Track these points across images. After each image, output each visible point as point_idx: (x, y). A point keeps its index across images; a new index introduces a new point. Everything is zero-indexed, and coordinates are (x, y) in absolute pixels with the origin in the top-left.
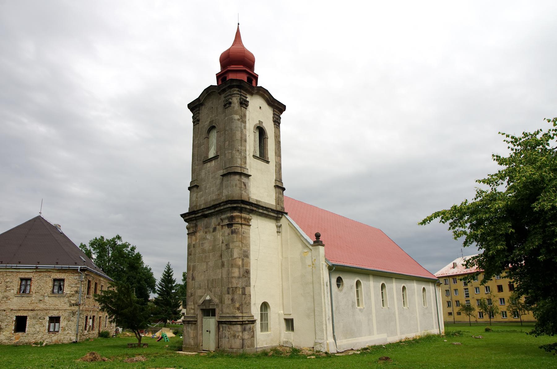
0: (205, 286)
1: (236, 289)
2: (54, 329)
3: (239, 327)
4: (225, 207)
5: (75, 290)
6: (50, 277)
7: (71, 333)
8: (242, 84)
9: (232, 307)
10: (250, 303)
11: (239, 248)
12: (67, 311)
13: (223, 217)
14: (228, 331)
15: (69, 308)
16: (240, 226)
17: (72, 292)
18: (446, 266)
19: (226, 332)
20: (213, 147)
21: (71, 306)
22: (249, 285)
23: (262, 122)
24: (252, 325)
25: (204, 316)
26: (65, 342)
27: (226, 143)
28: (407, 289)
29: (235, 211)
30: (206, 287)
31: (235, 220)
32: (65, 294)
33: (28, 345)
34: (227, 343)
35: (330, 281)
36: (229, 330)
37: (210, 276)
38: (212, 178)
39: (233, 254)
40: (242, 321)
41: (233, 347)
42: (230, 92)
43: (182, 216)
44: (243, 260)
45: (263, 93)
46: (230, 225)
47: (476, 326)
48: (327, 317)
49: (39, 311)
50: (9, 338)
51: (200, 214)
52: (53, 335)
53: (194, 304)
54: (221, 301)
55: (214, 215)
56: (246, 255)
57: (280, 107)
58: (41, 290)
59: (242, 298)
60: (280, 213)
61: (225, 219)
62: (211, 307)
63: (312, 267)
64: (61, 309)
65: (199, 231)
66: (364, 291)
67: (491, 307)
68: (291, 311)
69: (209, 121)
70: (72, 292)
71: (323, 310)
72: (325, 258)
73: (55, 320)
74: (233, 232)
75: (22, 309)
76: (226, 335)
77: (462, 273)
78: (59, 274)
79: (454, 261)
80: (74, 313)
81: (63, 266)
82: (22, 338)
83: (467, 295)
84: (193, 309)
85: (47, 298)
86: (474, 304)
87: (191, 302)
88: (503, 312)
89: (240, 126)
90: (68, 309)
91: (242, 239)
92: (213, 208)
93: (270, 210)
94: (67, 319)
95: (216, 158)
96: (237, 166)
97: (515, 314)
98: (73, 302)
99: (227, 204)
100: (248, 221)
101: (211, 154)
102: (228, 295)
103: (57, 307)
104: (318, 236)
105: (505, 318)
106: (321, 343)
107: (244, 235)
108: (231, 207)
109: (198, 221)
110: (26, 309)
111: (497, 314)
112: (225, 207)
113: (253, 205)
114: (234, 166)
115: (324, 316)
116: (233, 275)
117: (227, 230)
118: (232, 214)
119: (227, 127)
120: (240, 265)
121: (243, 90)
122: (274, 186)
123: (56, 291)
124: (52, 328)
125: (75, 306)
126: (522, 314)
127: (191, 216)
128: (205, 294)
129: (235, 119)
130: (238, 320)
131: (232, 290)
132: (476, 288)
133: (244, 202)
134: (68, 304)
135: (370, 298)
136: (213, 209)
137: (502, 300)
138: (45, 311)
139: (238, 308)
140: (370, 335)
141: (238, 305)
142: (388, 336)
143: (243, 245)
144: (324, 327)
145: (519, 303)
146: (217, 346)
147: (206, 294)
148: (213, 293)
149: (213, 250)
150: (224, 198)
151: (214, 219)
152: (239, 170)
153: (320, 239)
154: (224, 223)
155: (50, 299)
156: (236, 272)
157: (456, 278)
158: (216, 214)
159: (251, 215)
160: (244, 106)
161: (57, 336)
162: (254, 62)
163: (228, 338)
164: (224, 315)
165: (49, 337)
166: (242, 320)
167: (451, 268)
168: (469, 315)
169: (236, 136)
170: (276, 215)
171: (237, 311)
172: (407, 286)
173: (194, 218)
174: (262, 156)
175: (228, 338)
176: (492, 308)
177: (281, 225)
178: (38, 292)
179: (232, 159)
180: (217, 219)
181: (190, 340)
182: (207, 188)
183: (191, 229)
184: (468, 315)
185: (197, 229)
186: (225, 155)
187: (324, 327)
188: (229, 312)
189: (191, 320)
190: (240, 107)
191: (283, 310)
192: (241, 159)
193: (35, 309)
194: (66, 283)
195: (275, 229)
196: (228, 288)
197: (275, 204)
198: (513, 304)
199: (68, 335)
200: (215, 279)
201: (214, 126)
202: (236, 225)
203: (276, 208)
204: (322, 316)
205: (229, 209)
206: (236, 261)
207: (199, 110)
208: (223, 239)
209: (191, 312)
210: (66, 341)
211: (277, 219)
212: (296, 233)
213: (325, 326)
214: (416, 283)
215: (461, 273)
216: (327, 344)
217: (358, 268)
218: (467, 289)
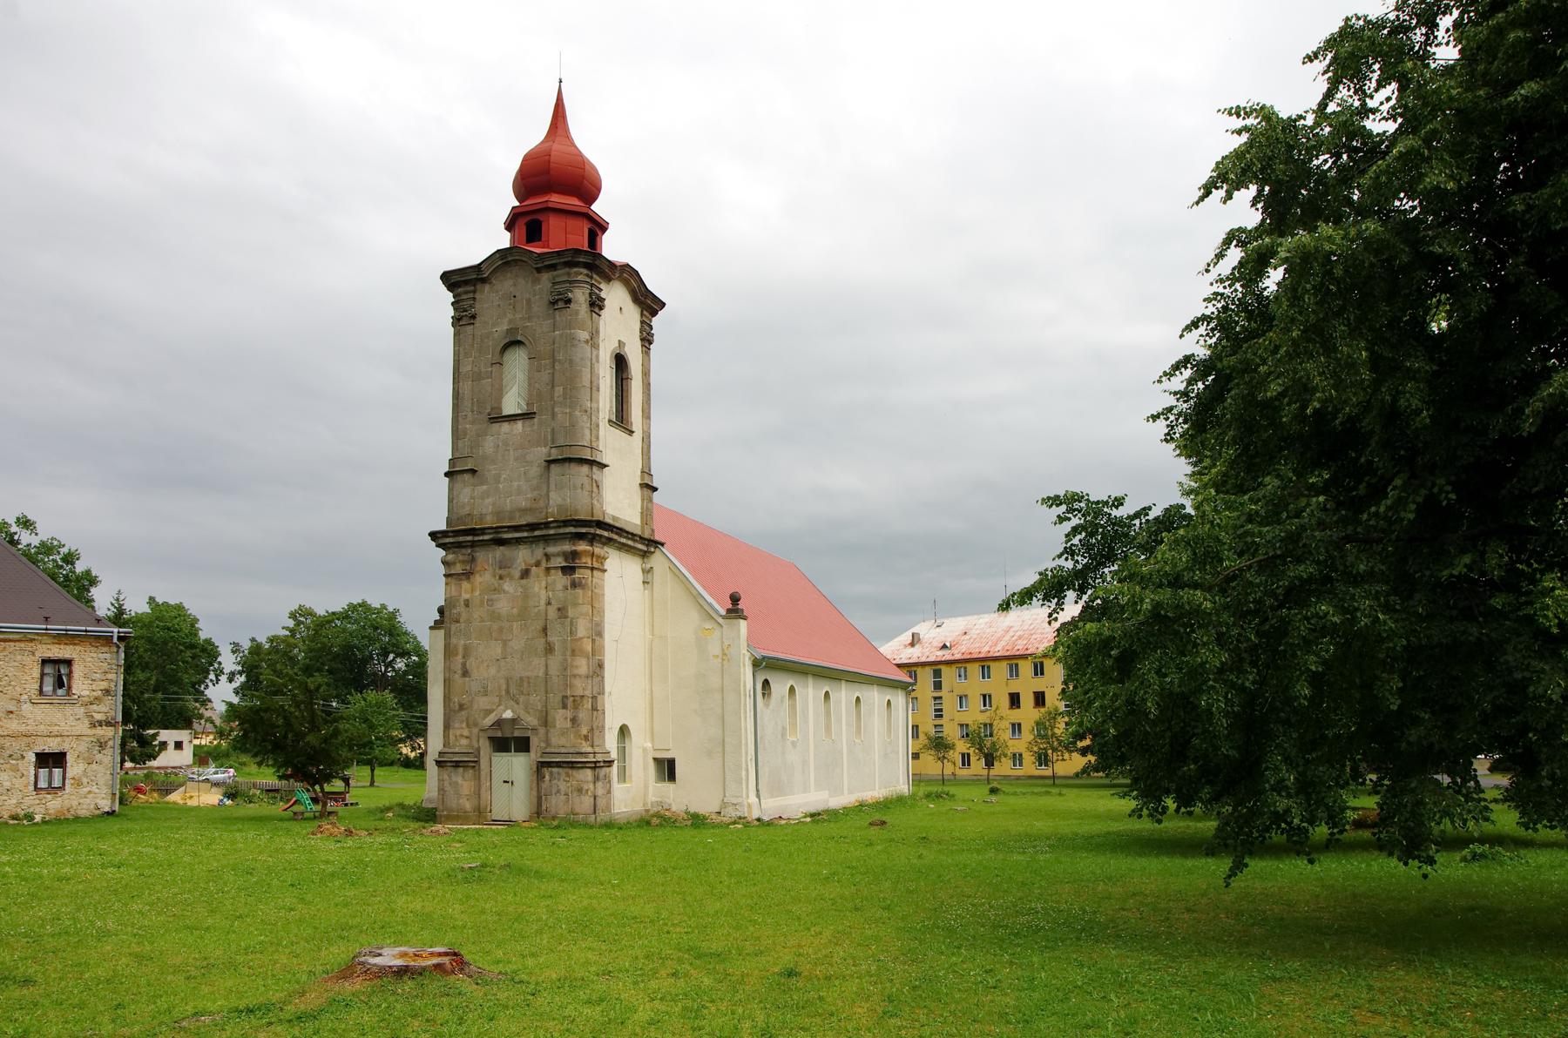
0: (500, 689)
2: (50, 783)
3: (588, 774)
4: (562, 531)
5: (102, 688)
6: (33, 654)
7: (97, 791)
10: (603, 727)
12: (84, 738)
13: (551, 549)
14: (564, 780)
17: (95, 693)
19: (559, 783)
21: (93, 725)
22: (602, 692)
23: (625, 344)
24: (607, 769)
26: (83, 813)
27: (557, 389)
29: (581, 542)
30: (504, 693)
31: (580, 559)
32: (76, 697)
34: (562, 804)
38: (516, 459)
40: (595, 762)
41: (577, 810)
42: (569, 274)
43: (434, 535)
44: (593, 641)
46: (568, 570)
53: (468, 726)
54: (546, 722)
55: (525, 542)
58: (10, 685)
61: (558, 555)
62: (516, 734)
63: (723, 660)
64: (69, 734)
67: (993, 744)
73: (52, 760)
74: (574, 585)
77: (932, 659)
78: (57, 646)
79: (915, 630)
80: (102, 745)
81: (68, 627)
83: (939, 714)
84: (467, 737)
85: (27, 707)
86: (951, 732)
88: (1014, 755)
92: (527, 528)
94: (84, 759)
95: (526, 416)
97: (1043, 759)
98: (98, 717)
99: (565, 526)
104: (735, 599)
105: (1018, 767)
106: (736, 805)
109: (477, 549)
111: (1003, 759)
112: (562, 531)
113: (615, 530)
116: (575, 672)
117: (560, 580)
118: (574, 548)
119: (559, 352)
121: (597, 274)
122: (640, 484)
123: (48, 688)
124: (45, 781)
125: (104, 727)
126: (1058, 760)
127: (461, 539)
128: (499, 706)
130: (588, 760)
131: (574, 701)
132: (961, 698)
133: (601, 524)
134: (87, 723)
136: (527, 531)
137: (1016, 728)
138: (25, 739)
139: (585, 736)
143: (595, 612)
144: (744, 773)
145: (1053, 735)
146: (535, 810)
147: (502, 707)
149: (523, 615)
150: (553, 511)
151: (524, 551)
155: (38, 710)
156: (582, 666)
159: (606, 549)
160: (597, 310)
161: (59, 799)
162: (599, 190)
164: (553, 750)
165: (38, 802)
166: (594, 760)
167: (906, 646)
170: (645, 548)
171: (583, 742)
173: (469, 544)
174: (621, 419)
176: (994, 745)
177: (652, 568)
179: (572, 428)
180: (532, 552)
182: (502, 479)
183: (458, 565)
185: (476, 566)
186: (554, 415)
189: (466, 759)
191: (652, 741)
194: (78, 670)
195: (639, 577)
196: (565, 697)
198: (1042, 737)
199: (90, 796)
200: (528, 678)
202: (582, 571)
206: (582, 643)
207: (474, 292)
208: (551, 596)
210: (84, 811)
211: (644, 555)
212: (688, 589)
215: (929, 660)
216: (749, 805)
218: (941, 698)
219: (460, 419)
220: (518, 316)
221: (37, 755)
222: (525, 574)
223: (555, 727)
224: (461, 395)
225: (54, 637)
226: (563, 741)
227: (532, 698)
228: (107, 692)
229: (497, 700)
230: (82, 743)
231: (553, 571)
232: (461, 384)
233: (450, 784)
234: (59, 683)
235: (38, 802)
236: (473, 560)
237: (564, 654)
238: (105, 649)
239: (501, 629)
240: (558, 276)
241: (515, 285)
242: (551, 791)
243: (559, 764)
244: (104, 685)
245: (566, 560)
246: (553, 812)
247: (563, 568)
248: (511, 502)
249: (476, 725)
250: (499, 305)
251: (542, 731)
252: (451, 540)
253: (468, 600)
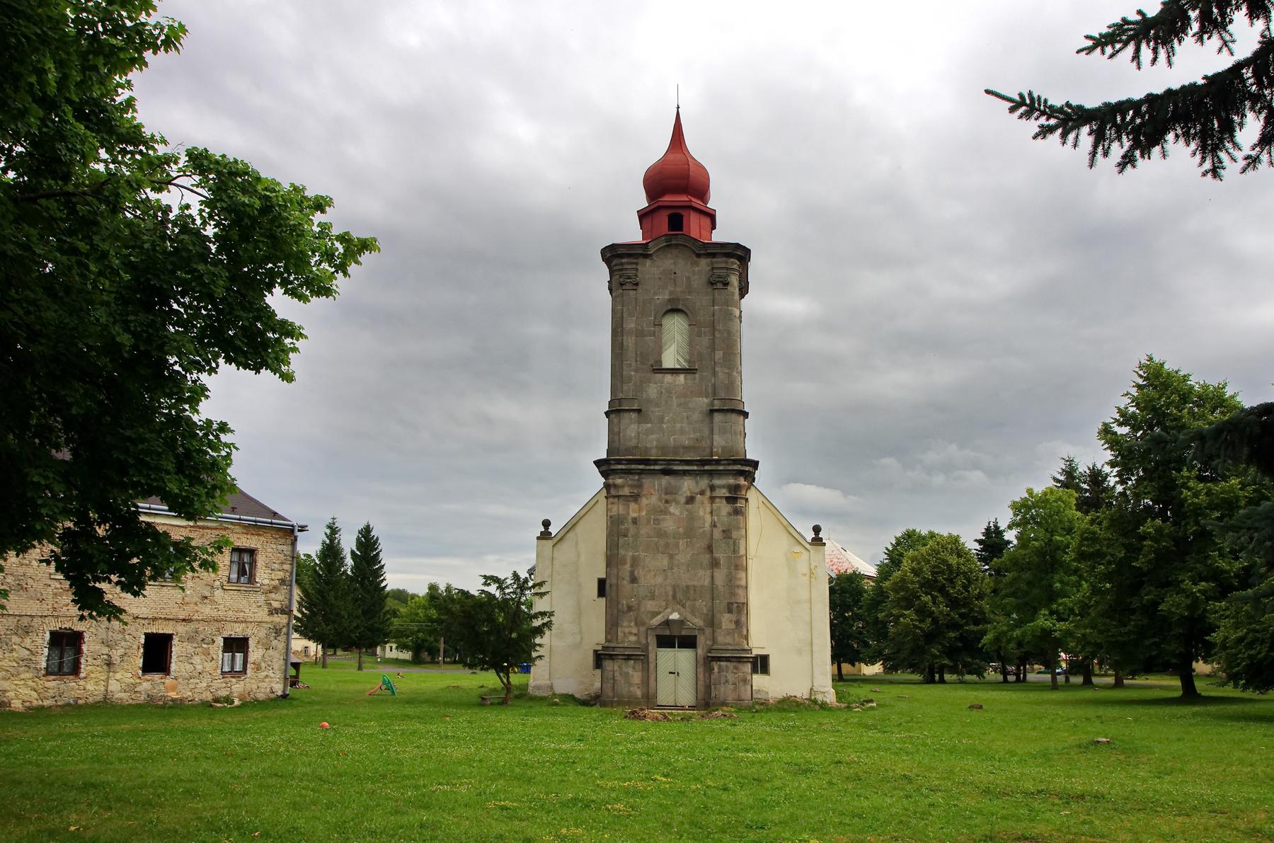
2: (232, 667)
4: (730, 468)
5: (280, 577)
7: (272, 675)
12: (264, 625)
13: (717, 482)
15: (268, 619)
17: (273, 582)
21: (271, 613)
26: (261, 696)
30: (670, 598)
33: (178, 706)
34: (730, 692)
38: (679, 405)
41: (743, 697)
42: (727, 263)
43: (598, 463)
46: (731, 500)
49: (201, 622)
50: (132, 688)
51: (657, 467)
52: (234, 680)
53: (636, 624)
54: (712, 623)
61: (723, 487)
62: (684, 633)
64: (252, 620)
70: (273, 582)
73: (236, 645)
75: (163, 617)
78: (245, 536)
81: (258, 519)
82: (72, 689)
84: (635, 635)
90: (265, 620)
94: (263, 645)
98: (276, 605)
103: (242, 614)
110: (171, 617)
112: (730, 468)
117: (725, 508)
123: (234, 576)
125: (279, 615)
128: (666, 608)
131: (738, 607)
136: (697, 465)
138: (216, 624)
147: (669, 610)
149: (690, 533)
151: (690, 482)
155: (227, 596)
161: (242, 682)
165: (224, 685)
178: (198, 577)
180: (697, 483)
193: (194, 618)
194: (261, 560)
199: (267, 680)
200: (694, 586)
207: (637, 264)
210: (262, 695)
219: (624, 367)
220: (678, 289)
221: (225, 639)
222: (690, 500)
223: (721, 628)
224: (625, 347)
225: (245, 527)
226: (729, 640)
227: (698, 603)
228: (282, 581)
229: (664, 604)
230: (262, 629)
231: (718, 500)
232: (625, 337)
233: (621, 674)
234: (242, 572)
235: (224, 685)
236: (640, 486)
237: (729, 568)
238: (282, 541)
239: (667, 545)
240: (717, 263)
241: (675, 264)
242: (720, 681)
243: (728, 659)
244: (281, 575)
245: (730, 492)
246: (721, 699)
247: (727, 498)
248: (674, 439)
249: (643, 624)
250: (660, 278)
251: (708, 631)
252: (623, 467)
253: (636, 519)
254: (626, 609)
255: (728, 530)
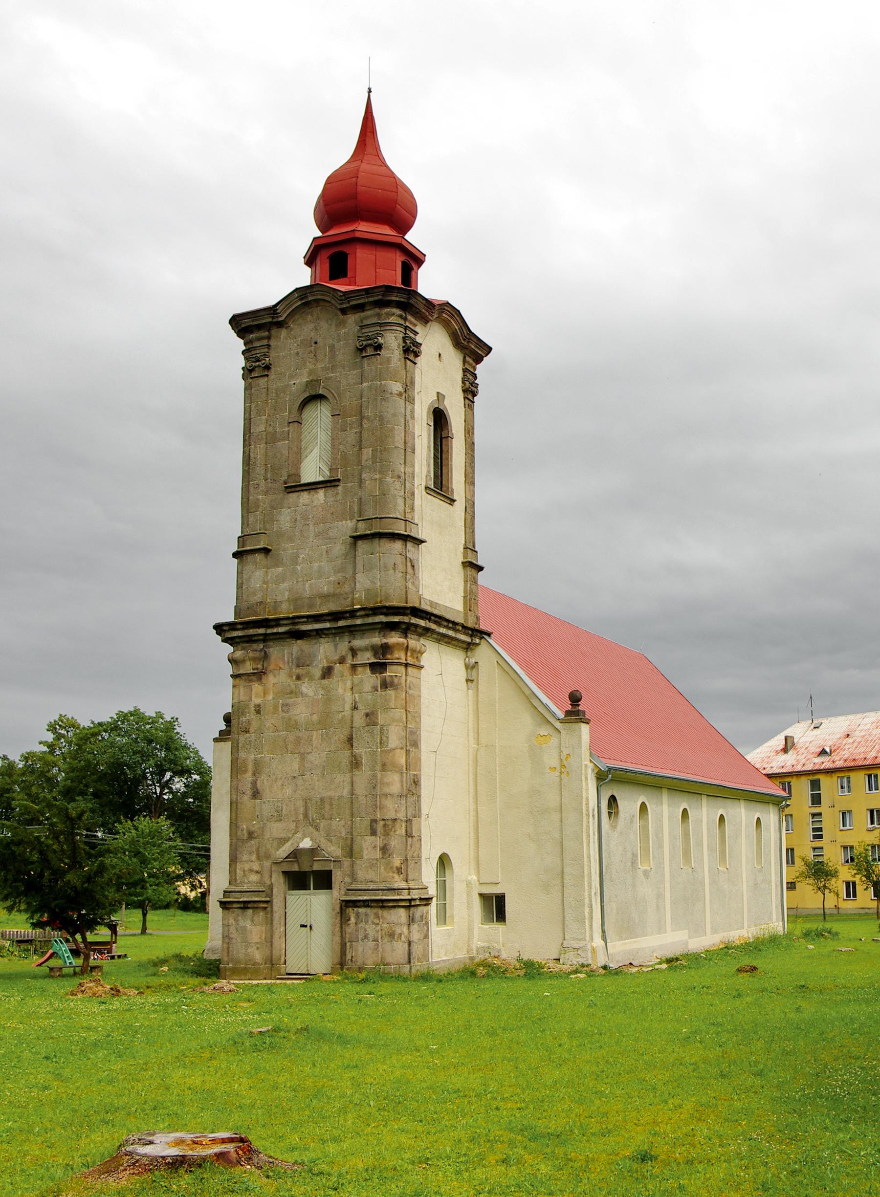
1: (394, 822)
3: (401, 914)
4: (370, 620)
8: (412, 301)
9: (382, 868)
10: (419, 857)
11: (400, 724)
13: (358, 643)
14: (373, 923)
16: (402, 669)
18: (764, 746)
19: (367, 926)
20: (316, 452)
22: (418, 814)
24: (424, 909)
25: (289, 890)
27: (365, 451)
28: (649, 810)
29: (393, 633)
30: (301, 817)
31: (391, 654)
34: (370, 952)
35: (598, 806)
36: (378, 922)
37: (313, 789)
38: (317, 535)
39: (387, 738)
40: (410, 900)
41: (389, 959)
43: (219, 628)
45: (449, 318)
46: (378, 667)
47: (837, 920)
48: (592, 887)
51: (281, 630)
54: (350, 852)
56: (412, 742)
57: (480, 352)
59: (407, 845)
60: (479, 635)
61: (366, 649)
62: (316, 867)
65: (276, 672)
66: (652, 828)
68: (500, 874)
69: (305, 379)
71: (586, 872)
72: (590, 752)
74: (385, 685)
76: (368, 934)
79: (788, 732)
83: (818, 834)
84: (257, 872)
86: (833, 856)
87: (251, 853)
89: (403, 412)
91: (406, 702)
92: (330, 618)
93: (461, 628)
95: (329, 484)
96: (397, 518)
99: (375, 614)
100: (417, 658)
101: (311, 471)
102: (373, 837)
104: (575, 699)
107: (411, 692)
108: (386, 622)
112: (370, 620)
114: (387, 516)
115: (586, 887)
116: (387, 790)
117: (369, 679)
118: (385, 641)
119: (367, 408)
120: (403, 767)
121: (412, 315)
122: (463, 563)
127: (251, 632)
129: (391, 394)
131: (385, 825)
132: (844, 814)
133: (417, 612)
135: (661, 846)
136: (330, 621)
140: (659, 933)
141: (399, 862)
142: (690, 938)
143: (409, 717)
144: (587, 910)
147: (299, 835)
148: (322, 832)
149: (325, 723)
151: (326, 645)
152: (400, 529)
153: (579, 705)
154: (359, 659)
156: (394, 783)
157: (789, 783)
158: (335, 633)
160: (411, 357)
163: (376, 940)
164: (360, 887)
166: (409, 897)
167: (777, 752)
168: (823, 889)
169: (394, 437)
170: (468, 640)
172: (762, 817)
175: (376, 940)
181: (249, 950)
182: (300, 560)
184: (819, 889)
187: (587, 910)
188: (375, 879)
189: (256, 899)
190: (403, 360)
192: (405, 499)
195: (462, 674)
196: (374, 821)
197: (462, 610)
201: (320, 394)
202: (394, 667)
203: (466, 619)
204: (583, 886)
205: (380, 626)
207: (269, 338)
209: (248, 879)
211: (468, 647)
213: (588, 909)
214: (745, 808)
215: (806, 768)
217: (645, 774)
218: (820, 814)
222: (327, 672)
229: (293, 826)
239: (298, 740)
254: (246, 836)
255: (373, 713)
